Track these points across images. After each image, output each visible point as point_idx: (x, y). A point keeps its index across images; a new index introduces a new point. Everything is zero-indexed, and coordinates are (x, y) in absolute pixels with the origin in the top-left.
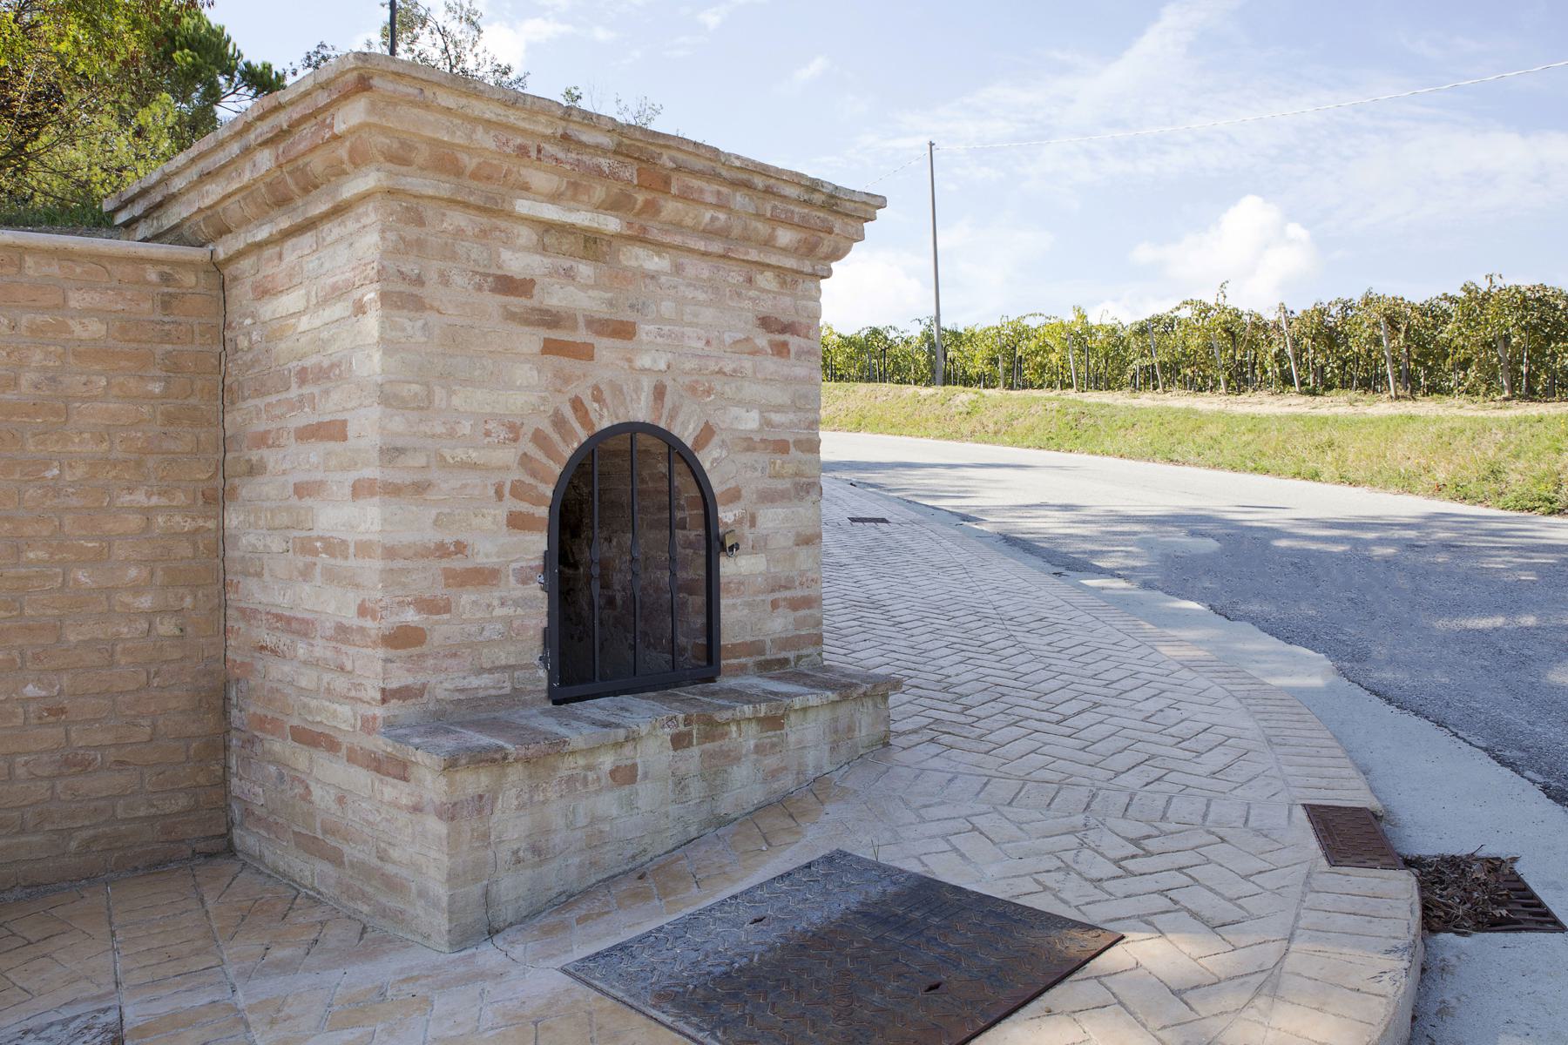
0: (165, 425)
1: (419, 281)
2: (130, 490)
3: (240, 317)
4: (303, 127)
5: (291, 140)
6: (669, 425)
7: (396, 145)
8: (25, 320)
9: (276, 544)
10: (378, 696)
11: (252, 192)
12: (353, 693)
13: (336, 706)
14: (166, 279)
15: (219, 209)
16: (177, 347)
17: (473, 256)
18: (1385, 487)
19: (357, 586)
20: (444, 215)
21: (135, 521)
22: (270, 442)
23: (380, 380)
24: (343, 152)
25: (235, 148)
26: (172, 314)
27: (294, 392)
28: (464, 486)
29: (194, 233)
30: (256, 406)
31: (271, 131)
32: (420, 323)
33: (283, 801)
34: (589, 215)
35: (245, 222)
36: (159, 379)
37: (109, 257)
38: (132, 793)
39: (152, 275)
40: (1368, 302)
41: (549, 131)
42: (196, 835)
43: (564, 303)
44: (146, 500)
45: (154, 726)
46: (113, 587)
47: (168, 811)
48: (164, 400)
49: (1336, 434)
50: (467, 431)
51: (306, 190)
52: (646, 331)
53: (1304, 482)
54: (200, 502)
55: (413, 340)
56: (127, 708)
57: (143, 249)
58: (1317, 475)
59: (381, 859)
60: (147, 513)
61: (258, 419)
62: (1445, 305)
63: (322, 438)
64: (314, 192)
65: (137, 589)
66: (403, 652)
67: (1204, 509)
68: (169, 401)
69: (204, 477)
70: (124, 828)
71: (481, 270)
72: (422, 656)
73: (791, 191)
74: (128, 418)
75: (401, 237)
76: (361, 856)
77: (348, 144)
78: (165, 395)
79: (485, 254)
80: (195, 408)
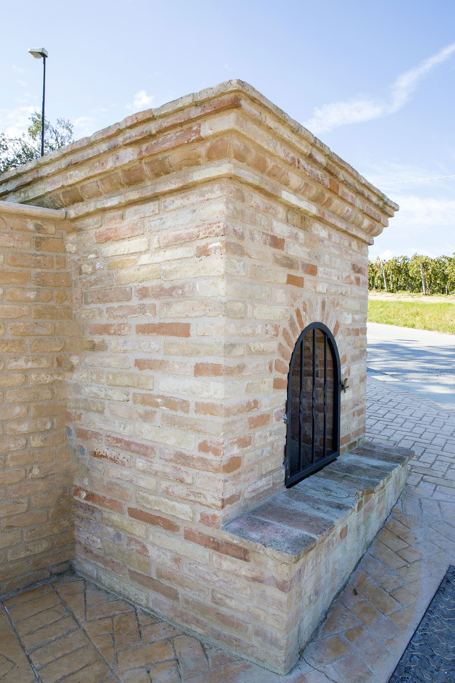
0: (36, 318)
1: (242, 237)
2: (16, 359)
3: (84, 253)
4: (168, 133)
5: (155, 141)
6: (326, 323)
7: (242, 148)
8: (326, 269)
9: (117, 395)
10: (219, 504)
11: (109, 176)
12: (192, 498)
13: (174, 503)
14: (38, 228)
15: (78, 187)
16: (44, 270)
17: (263, 223)
18: (444, 331)
19: (199, 431)
20: (252, 196)
21: (18, 378)
22: (112, 331)
23: (224, 300)
24: (202, 150)
25: (104, 147)
26: (41, 250)
27: (135, 302)
28: (258, 365)
29: (53, 202)
30: (99, 309)
31: (140, 135)
32: (242, 263)
33: (119, 550)
34: (306, 204)
35: (98, 194)
36: (34, 290)
37: (6, 213)
38: (16, 544)
39: (31, 226)
40: (415, 258)
41: (306, 151)
42: (53, 564)
43: (294, 254)
44: (25, 365)
45: (29, 502)
46: (5, 420)
47: (37, 552)
48: (36, 303)
49: (419, 310)
50: (260, 332)
51: (157, 175)
52: (320, 269)
53: (408, 328)
54: (55, 365)
55: (240, 274)
56: (14, 493)
57: (28, 209)
58: (414, 325)
59: (217, 603)
60: (25, 372)
61: (101, 317)
62: (443, 260)
63: (163, 333)
64: (164, 177)
65: (19, 420)
66: (231, 474)
67: (389, 341)
68: (38, 303)
69: (58, 349)
70: (11, 566)
71: (265, 232)
72: (239, 474)
73: (374, 199)
74: (15, 314)
75: (235, 208)
76: (196, 597)
77: (208, 144)
78: (36, 300)
79: (267, 222)
80: (54, 308)
